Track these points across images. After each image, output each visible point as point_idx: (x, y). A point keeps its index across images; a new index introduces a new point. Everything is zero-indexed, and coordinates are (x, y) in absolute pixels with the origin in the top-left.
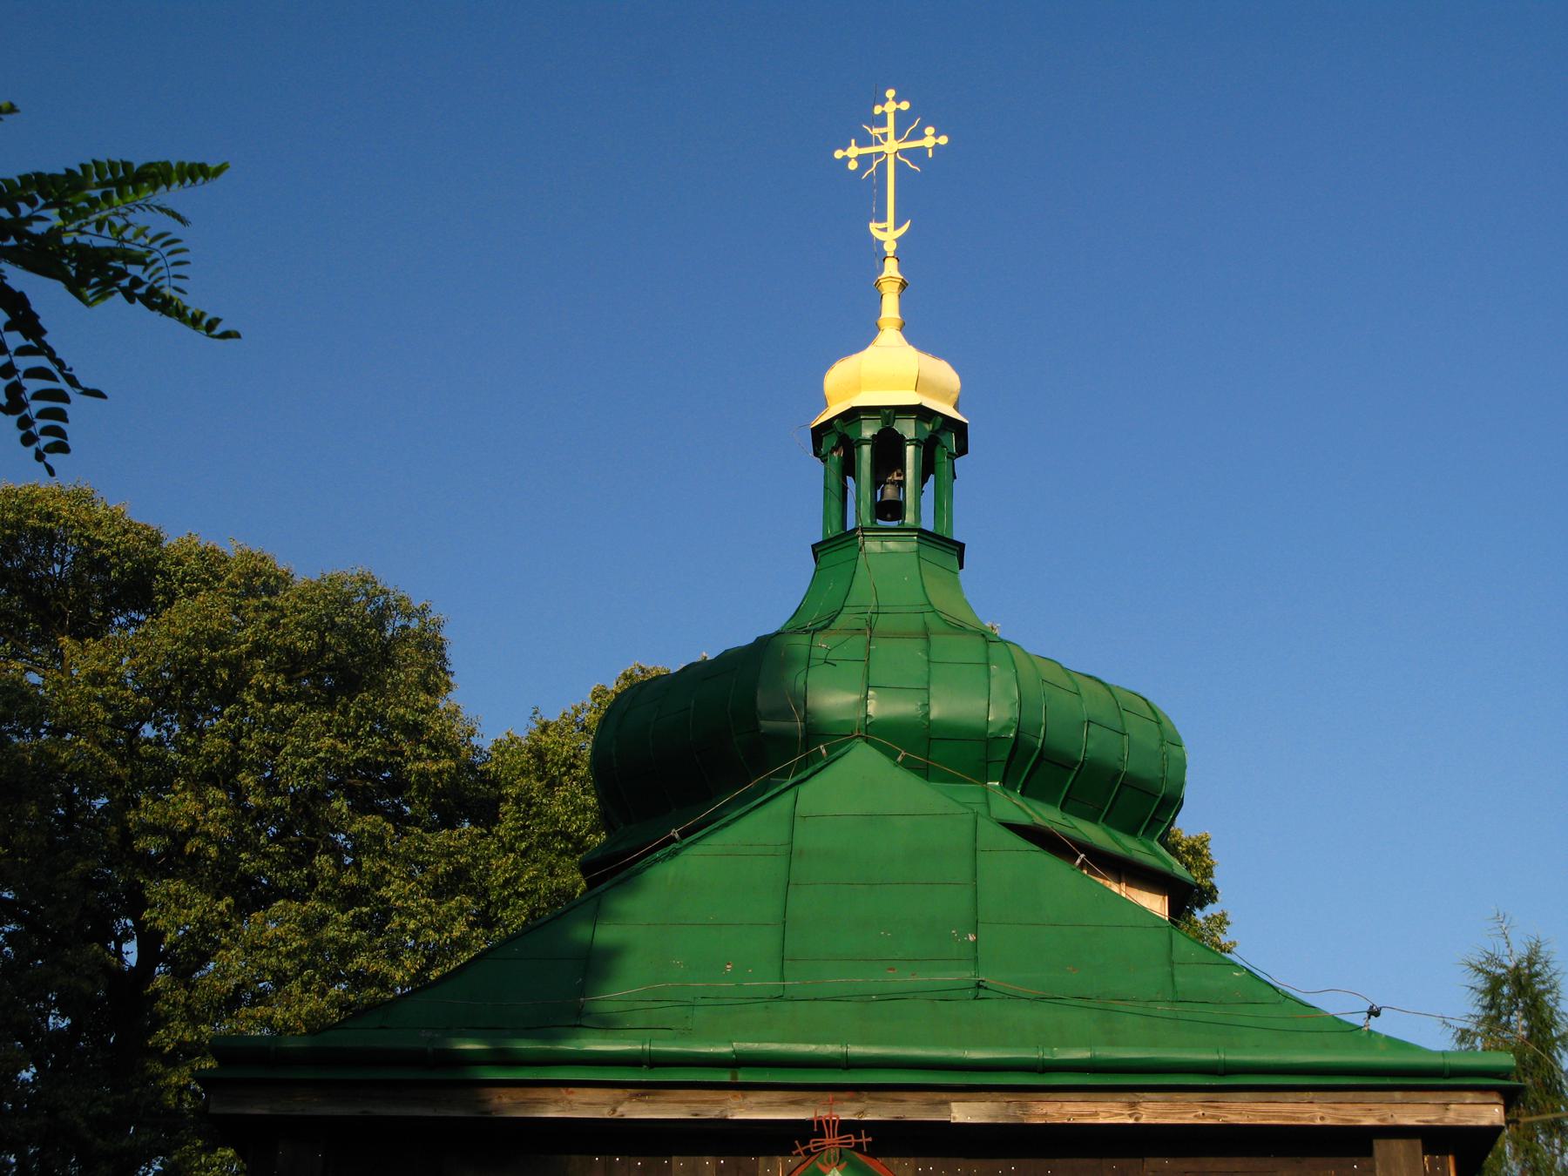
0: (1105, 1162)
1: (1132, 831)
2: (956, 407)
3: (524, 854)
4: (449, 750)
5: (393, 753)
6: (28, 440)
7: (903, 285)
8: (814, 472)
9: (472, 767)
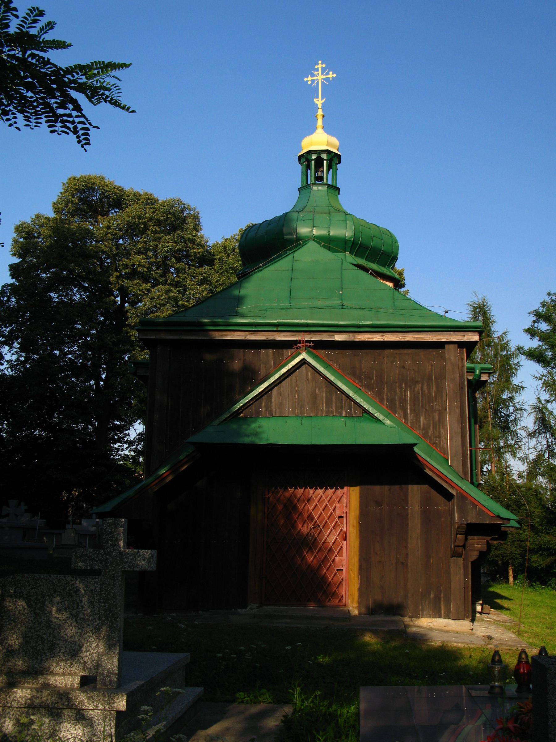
0: (375, 350)
1: (384, 266)
2: (338, 150)
3: (221, 273)
4: (202, 246)
5: (187, 247)
6: (79, 142)
7: (323, 116)
8: (299, 168)
9: (207, 251)
